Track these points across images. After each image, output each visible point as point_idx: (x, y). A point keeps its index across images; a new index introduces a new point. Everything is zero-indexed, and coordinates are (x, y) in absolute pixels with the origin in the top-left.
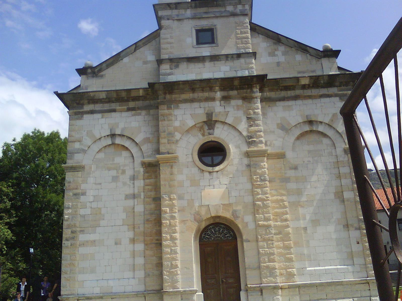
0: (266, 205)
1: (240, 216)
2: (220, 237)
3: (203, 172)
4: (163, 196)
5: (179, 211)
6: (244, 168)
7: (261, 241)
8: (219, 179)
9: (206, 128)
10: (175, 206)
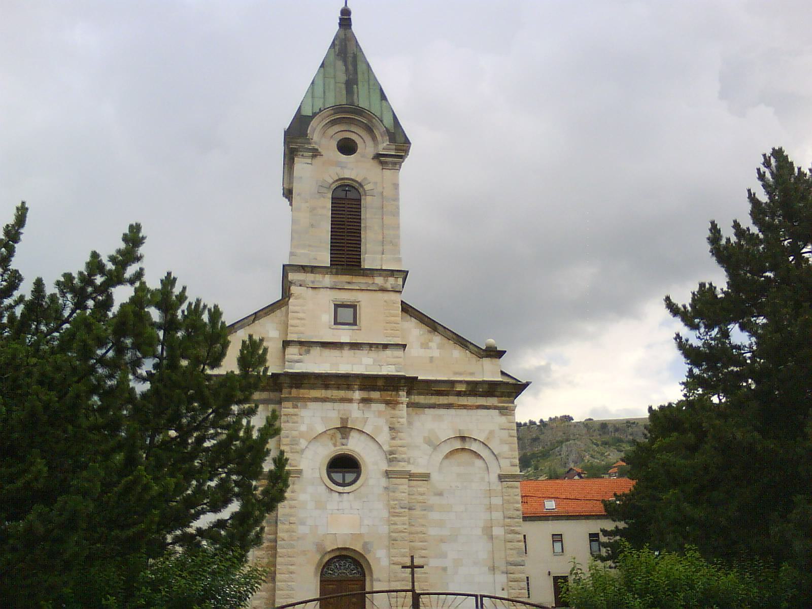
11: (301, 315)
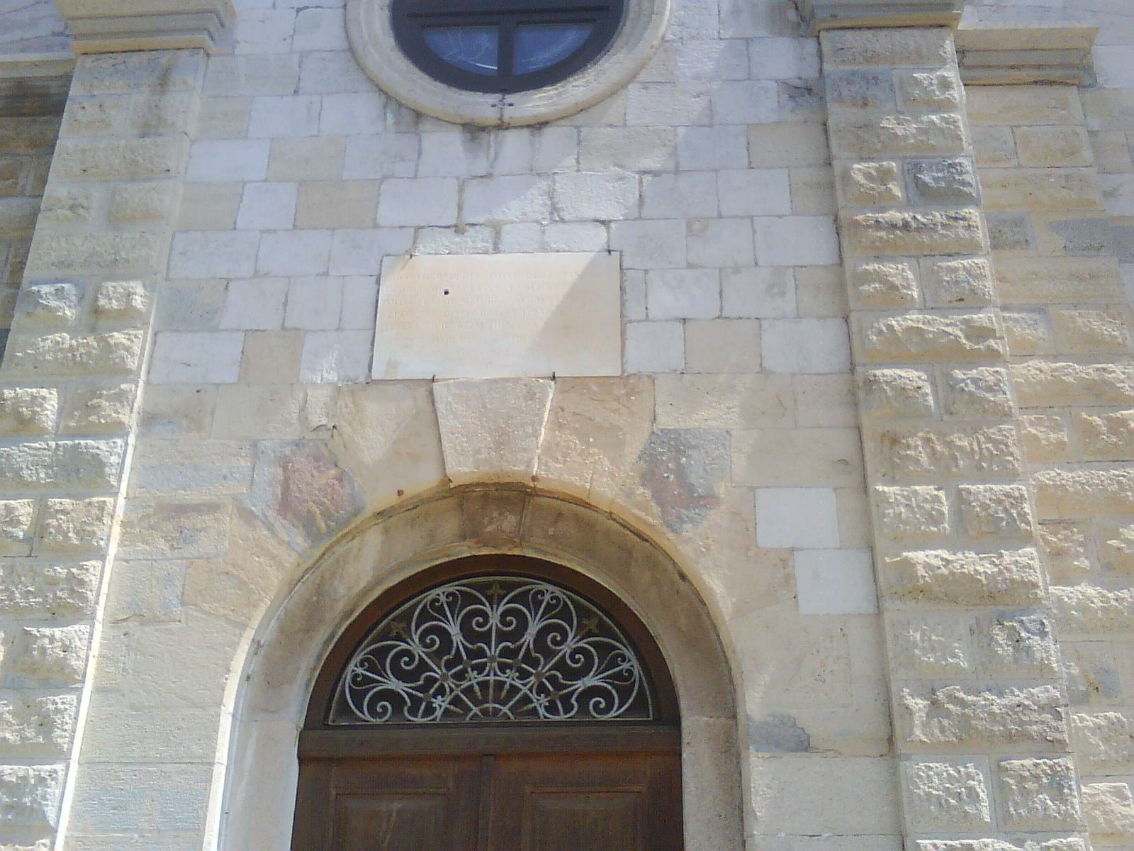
0: (973, 399)
1: (721, 490)
2: (514, 690)
3: (417, 123)
4: (35, 288)
5: (149, 420)
6: (769, 107)
7: (936, 750)
8: (543, 184)
10: (126, 374)
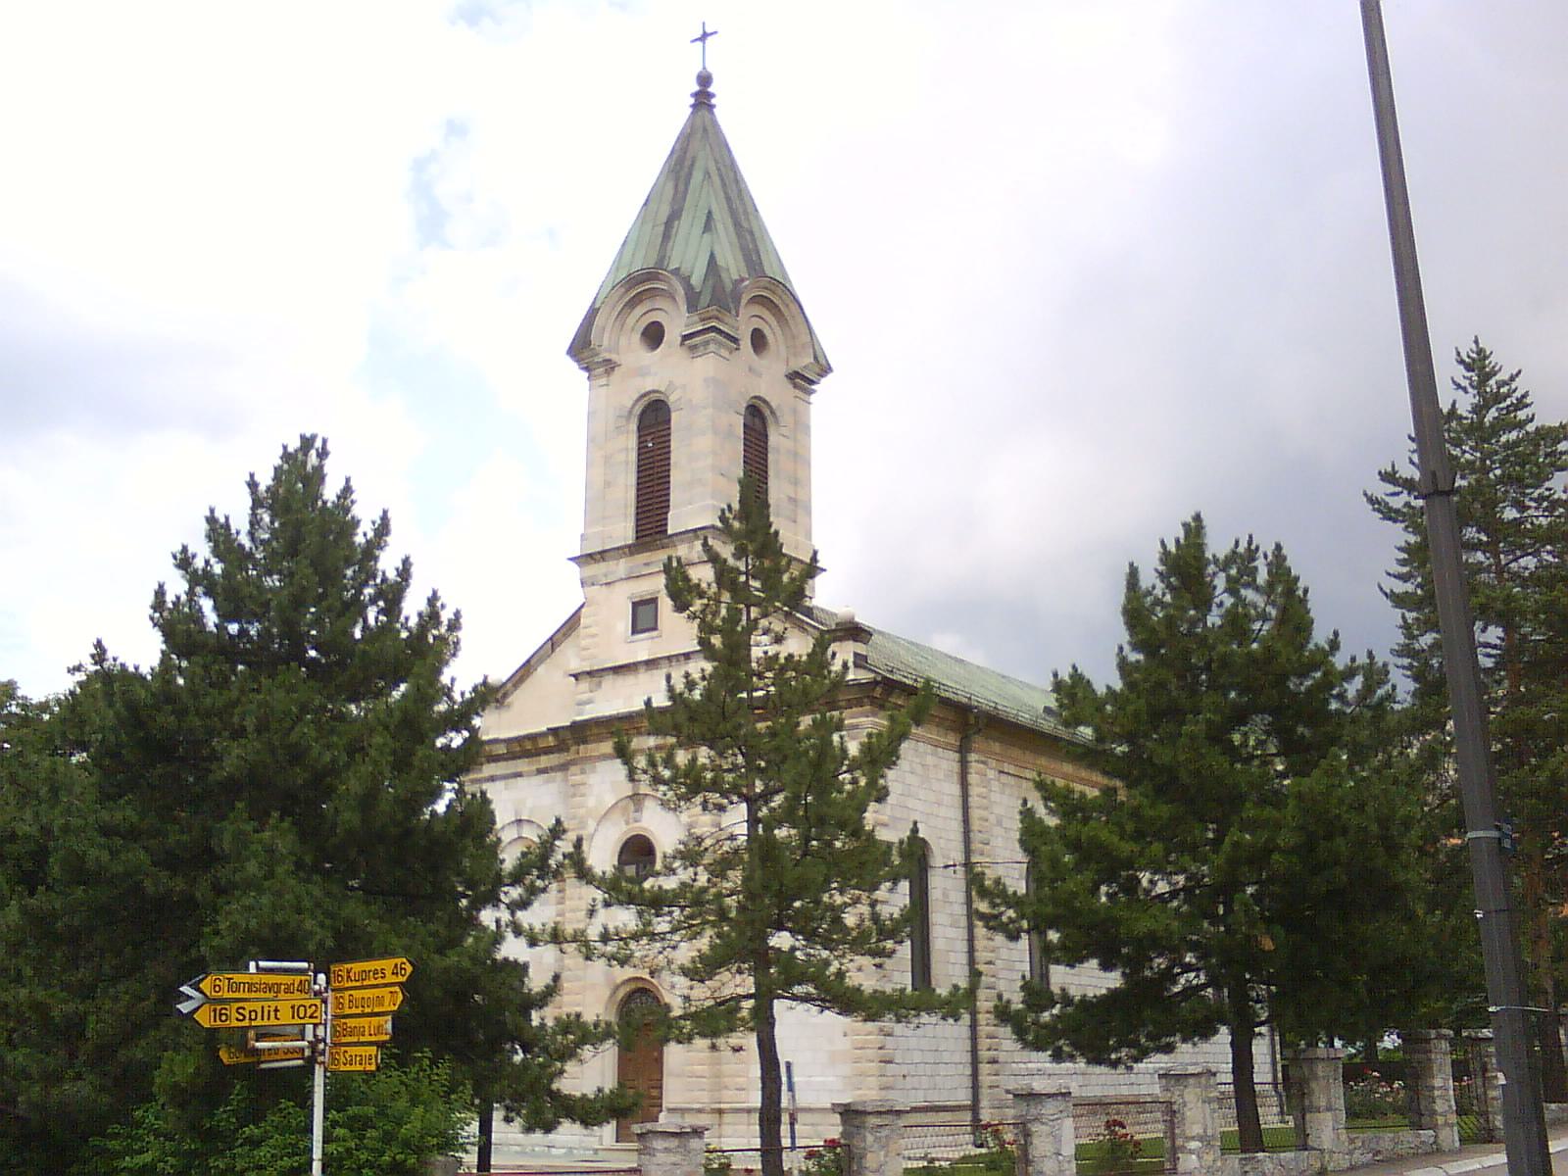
9: (632, 807)
11: (593, 630)
